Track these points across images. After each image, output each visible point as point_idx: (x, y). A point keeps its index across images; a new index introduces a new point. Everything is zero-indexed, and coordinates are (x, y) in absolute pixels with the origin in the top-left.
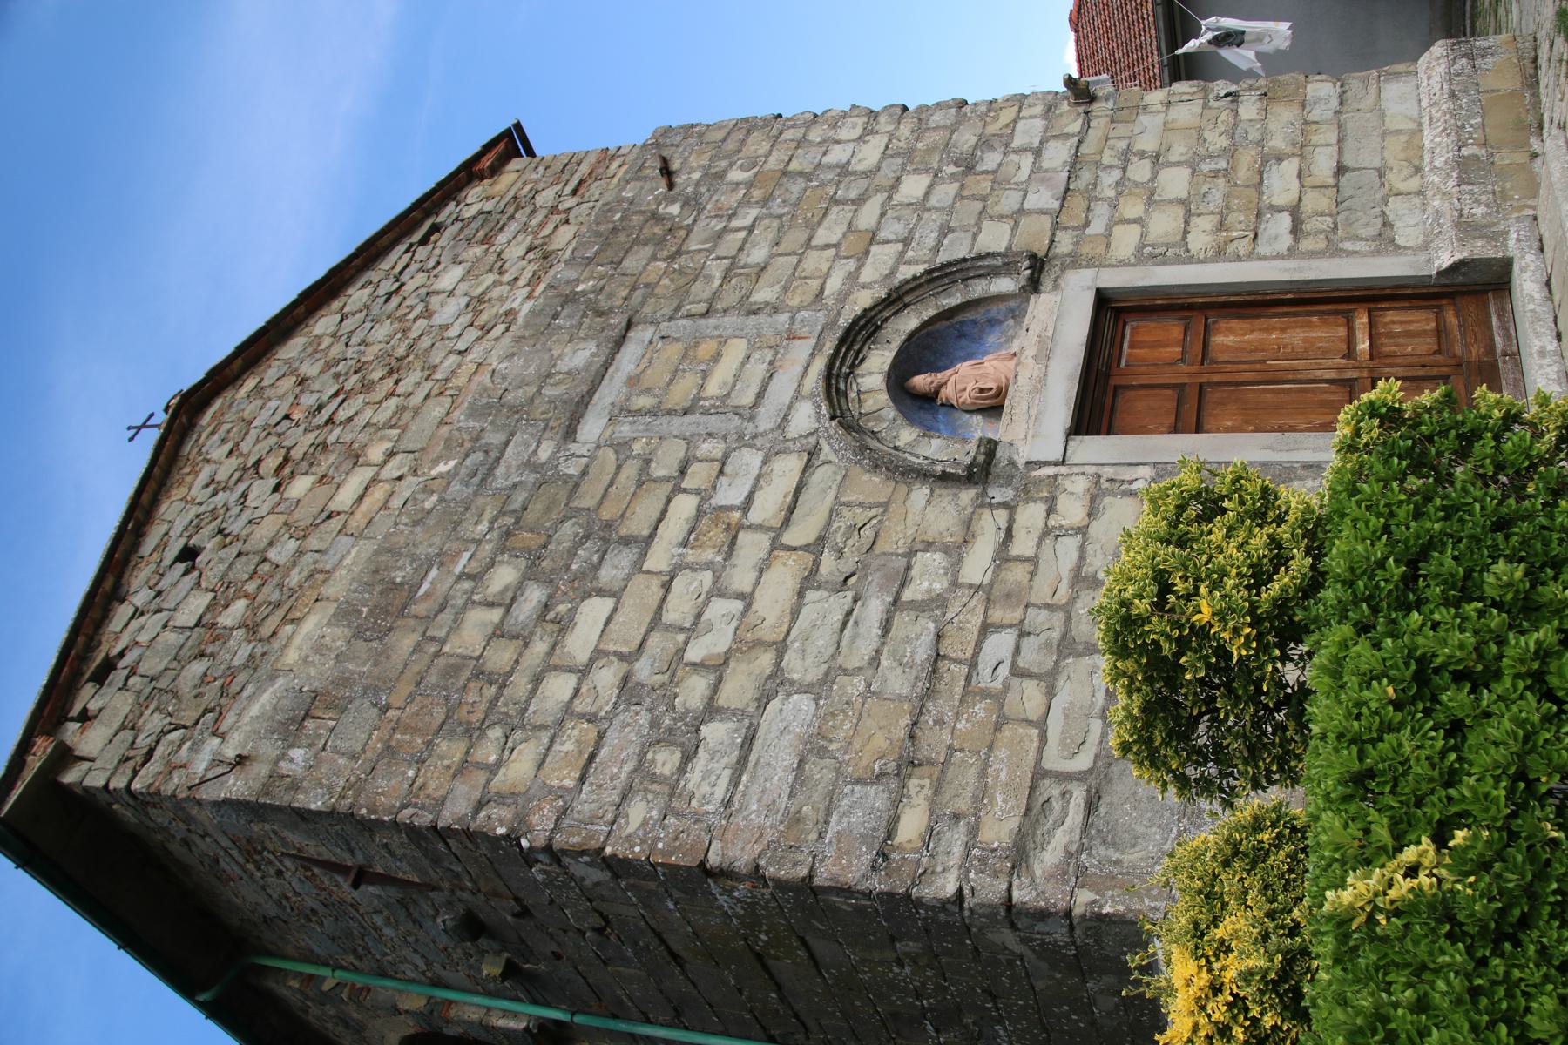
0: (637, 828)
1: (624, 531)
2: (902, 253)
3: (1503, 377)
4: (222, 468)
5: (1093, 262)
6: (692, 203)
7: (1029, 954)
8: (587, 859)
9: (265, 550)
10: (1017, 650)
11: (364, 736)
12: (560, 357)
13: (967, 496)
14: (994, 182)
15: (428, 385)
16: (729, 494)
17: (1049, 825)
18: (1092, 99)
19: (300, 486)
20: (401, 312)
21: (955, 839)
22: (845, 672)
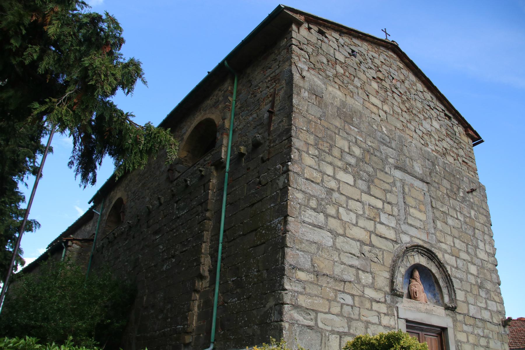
0: (295, 196)
1: (371, 186)
2: (453, 267)
4: (377, 60)
5: (455, 326)
6: (464, 200)
7: (266, 309)
8: (286, 182)
9: (357, 77)
10: (348, 305)
11: (312, 113)
12: (417, 162)
13: (387, 289)
14: (476, 295)
15: (405, 122)
16: (384, 218)
17: (304, 315)
18: (504, 326)
19: (375, 85)
20: (425, 110)
21: (299, 288)
22: (339, 255)
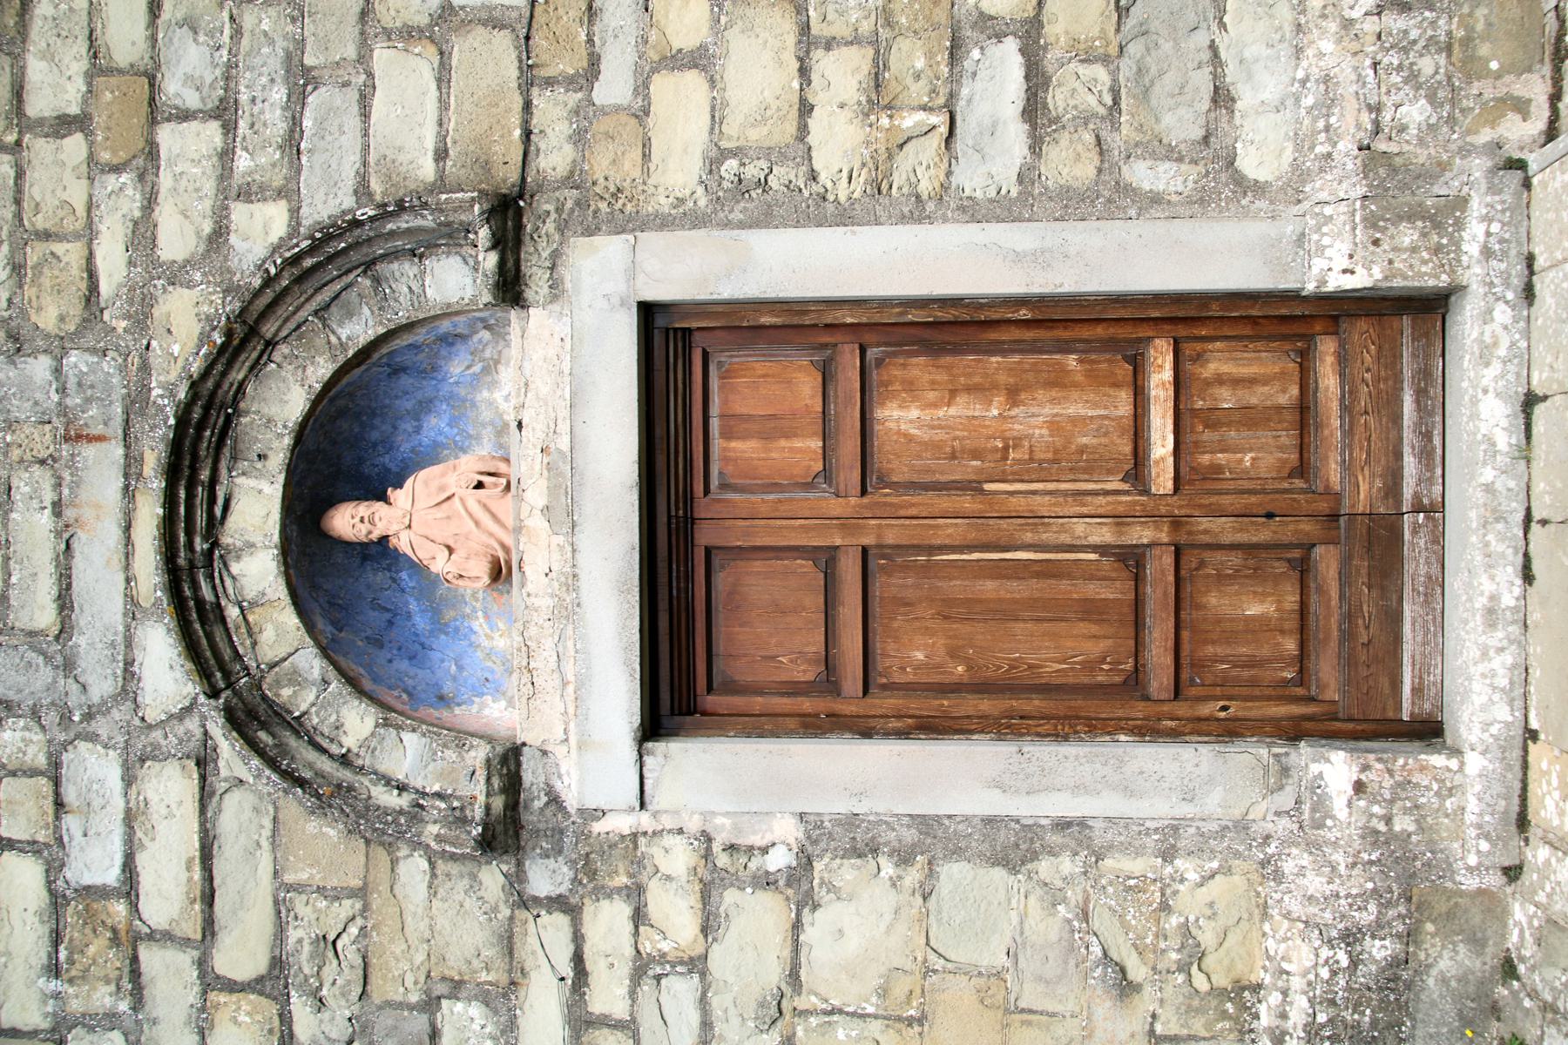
3: (1409, 568)
